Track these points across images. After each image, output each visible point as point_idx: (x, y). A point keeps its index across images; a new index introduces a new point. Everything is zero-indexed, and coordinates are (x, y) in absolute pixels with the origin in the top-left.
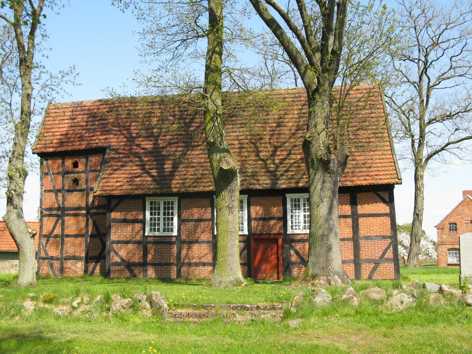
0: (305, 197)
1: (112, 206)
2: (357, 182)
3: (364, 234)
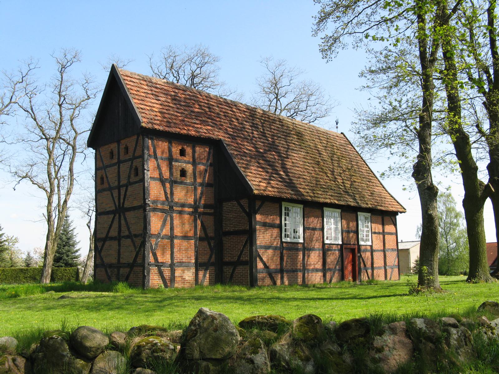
1: (257, 208)
2: (391, 208)
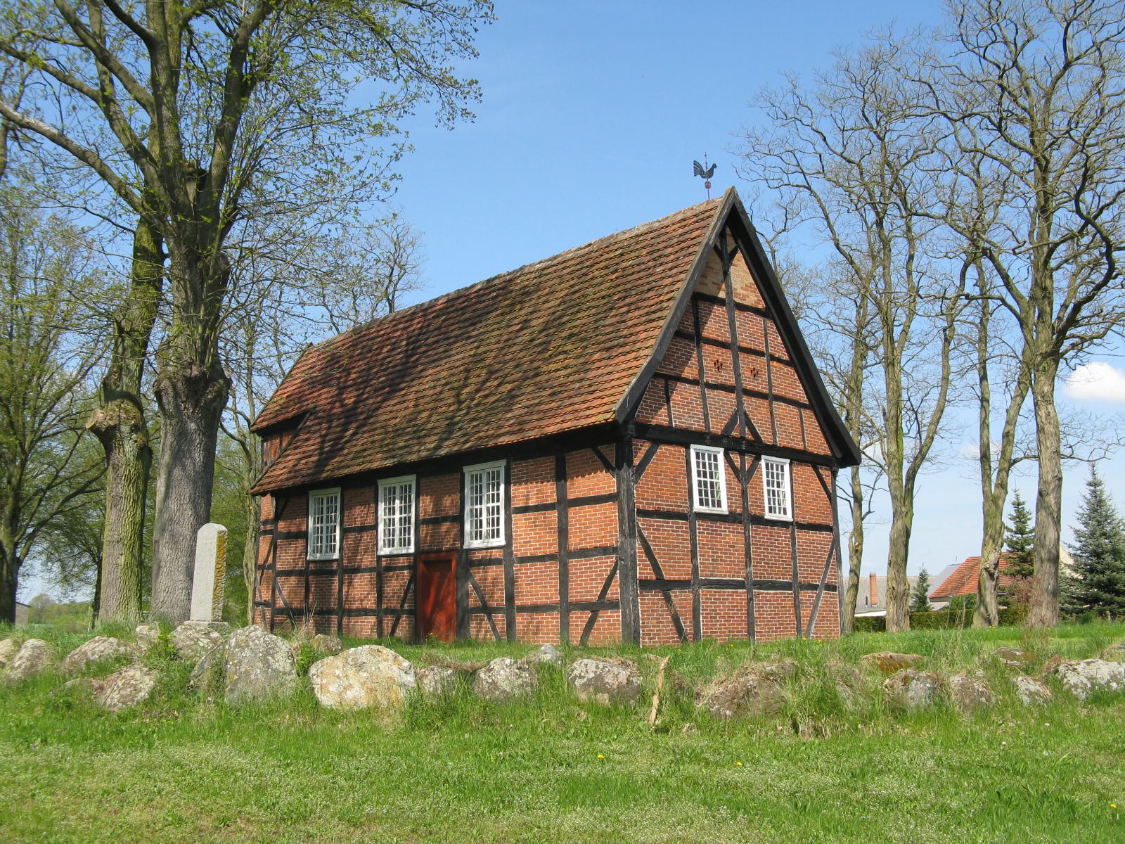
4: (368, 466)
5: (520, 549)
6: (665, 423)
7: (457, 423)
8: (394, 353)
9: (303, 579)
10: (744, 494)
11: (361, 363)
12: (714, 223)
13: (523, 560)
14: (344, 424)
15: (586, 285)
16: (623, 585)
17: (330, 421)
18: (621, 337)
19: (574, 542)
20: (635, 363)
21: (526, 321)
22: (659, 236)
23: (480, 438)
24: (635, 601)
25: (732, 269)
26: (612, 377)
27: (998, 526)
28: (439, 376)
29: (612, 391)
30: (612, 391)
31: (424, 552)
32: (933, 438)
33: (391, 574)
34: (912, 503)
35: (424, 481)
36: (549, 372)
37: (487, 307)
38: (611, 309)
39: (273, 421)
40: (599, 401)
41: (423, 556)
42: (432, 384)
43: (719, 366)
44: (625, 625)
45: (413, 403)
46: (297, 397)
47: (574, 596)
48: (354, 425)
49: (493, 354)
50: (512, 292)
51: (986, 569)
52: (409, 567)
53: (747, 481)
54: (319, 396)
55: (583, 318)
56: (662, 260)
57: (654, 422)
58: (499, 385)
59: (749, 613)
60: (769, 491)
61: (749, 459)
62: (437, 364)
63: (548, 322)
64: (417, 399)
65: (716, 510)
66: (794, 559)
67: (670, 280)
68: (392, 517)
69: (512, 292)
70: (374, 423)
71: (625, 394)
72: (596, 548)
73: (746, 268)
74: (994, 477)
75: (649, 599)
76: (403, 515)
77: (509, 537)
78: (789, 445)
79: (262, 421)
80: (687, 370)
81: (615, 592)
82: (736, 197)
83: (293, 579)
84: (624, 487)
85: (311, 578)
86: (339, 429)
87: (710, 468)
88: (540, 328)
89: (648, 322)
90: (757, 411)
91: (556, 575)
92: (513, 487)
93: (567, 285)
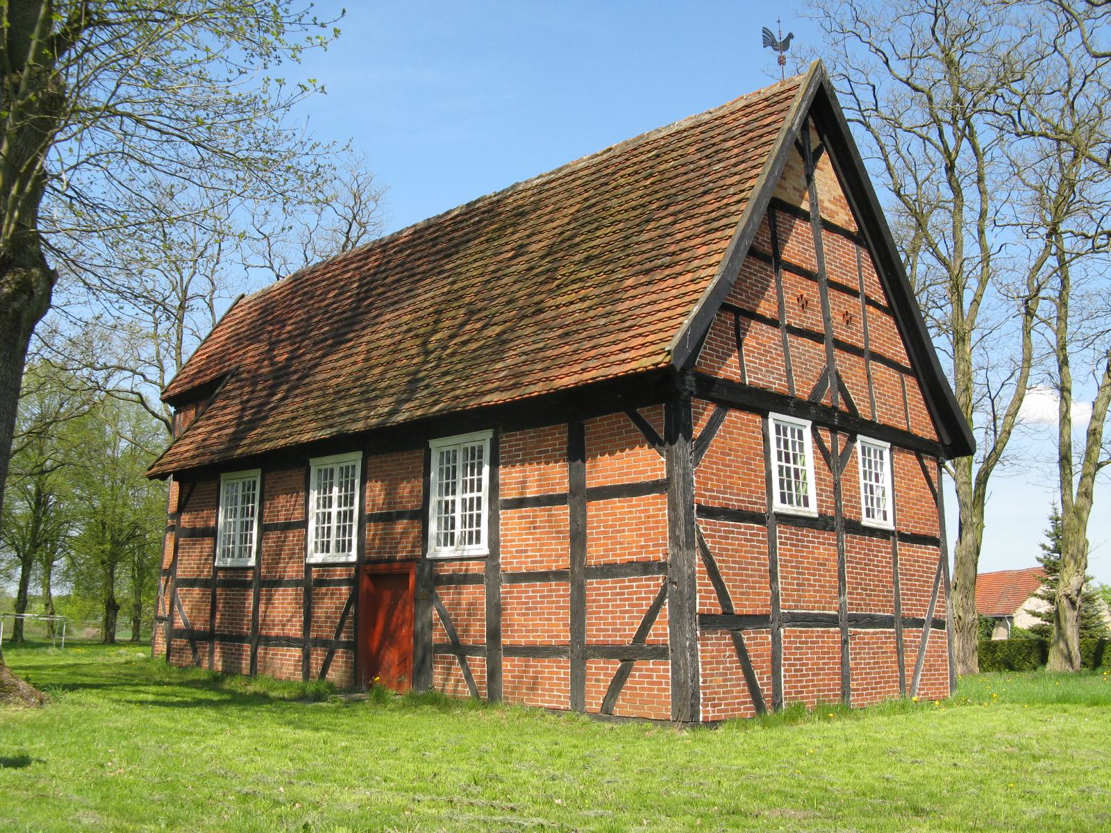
0: (466, 445)
3: (598, 557)
4: (297, 438)
5: (510, 561)
6: (736, 378)
7: (422, 379)
8: (342, 298)
9: (209, 592)
10: (836, 487)
11: (299, 312)
12: (793, 116)
13: (516, 578)
14: (271, 387)
15: (607, 196)
16: (675, 622)
17: (255, 384)
18: (667, 255)
19: (596, 553)
20: (692, 287)
21: (521, 246)
22: (711, 129)
23: (457, 397)
24: (693, 648)
25: (817, 173)
26: (657, 307)
27: (1081, 544)
28: (399, 321)
29: (660, 326)
30: (660, 326)
31: (370, 561)
32: (1009, 433)
33: (324, 590)
34: (982, 513)
35: (372, 460)
36: (558, 307)
37: (466, 234)
38: (648, 221)
39: (188, 387)
40: (640, 340)
41: (368, 567)
42: (389, 332)
43: (804, 304)
44: (678, 685)
45: (362, 357)
46: (221, 357)
47: (593, 635)
48: (285, 387)
49: (475, 290)
50: (501, 213)
51: (1067, 596)
52: (348, 582)
53: (840, 469)
54: (245, 353)
55: (604, 236)
56: (720, 156)
57: (722, 374)
58: (484, 327)
59: (844, 663)
60: (866, 485)
61: (842, 439)
62: (397, 306)
63: (553, 244)
64: (368, 351)
65: (801, 511)
66: (896, 583)
67: (737, 178)
68: (327, 510)
69: (501, 213)
70: (309, 384)
71: (684, 328)
72: (631, 563)
73: (833, 174)
74: (1076, 480)
75: (712, 645)
76: (343, 509)
77: (494, 544)
78: (891, 423)
79: (176, 387)
80: (763, 303)
81: (660, 632)
82: (823, 75)
83: (196, 591)
84: (678, 470)
85: (219, 591)
86: (264, 393)
87: (794, 449)
88: (541, 253)
89: (708, 232)
90: (850, 369)
91: (565, 602)
92: (502, 470)
93: (579, 199)
